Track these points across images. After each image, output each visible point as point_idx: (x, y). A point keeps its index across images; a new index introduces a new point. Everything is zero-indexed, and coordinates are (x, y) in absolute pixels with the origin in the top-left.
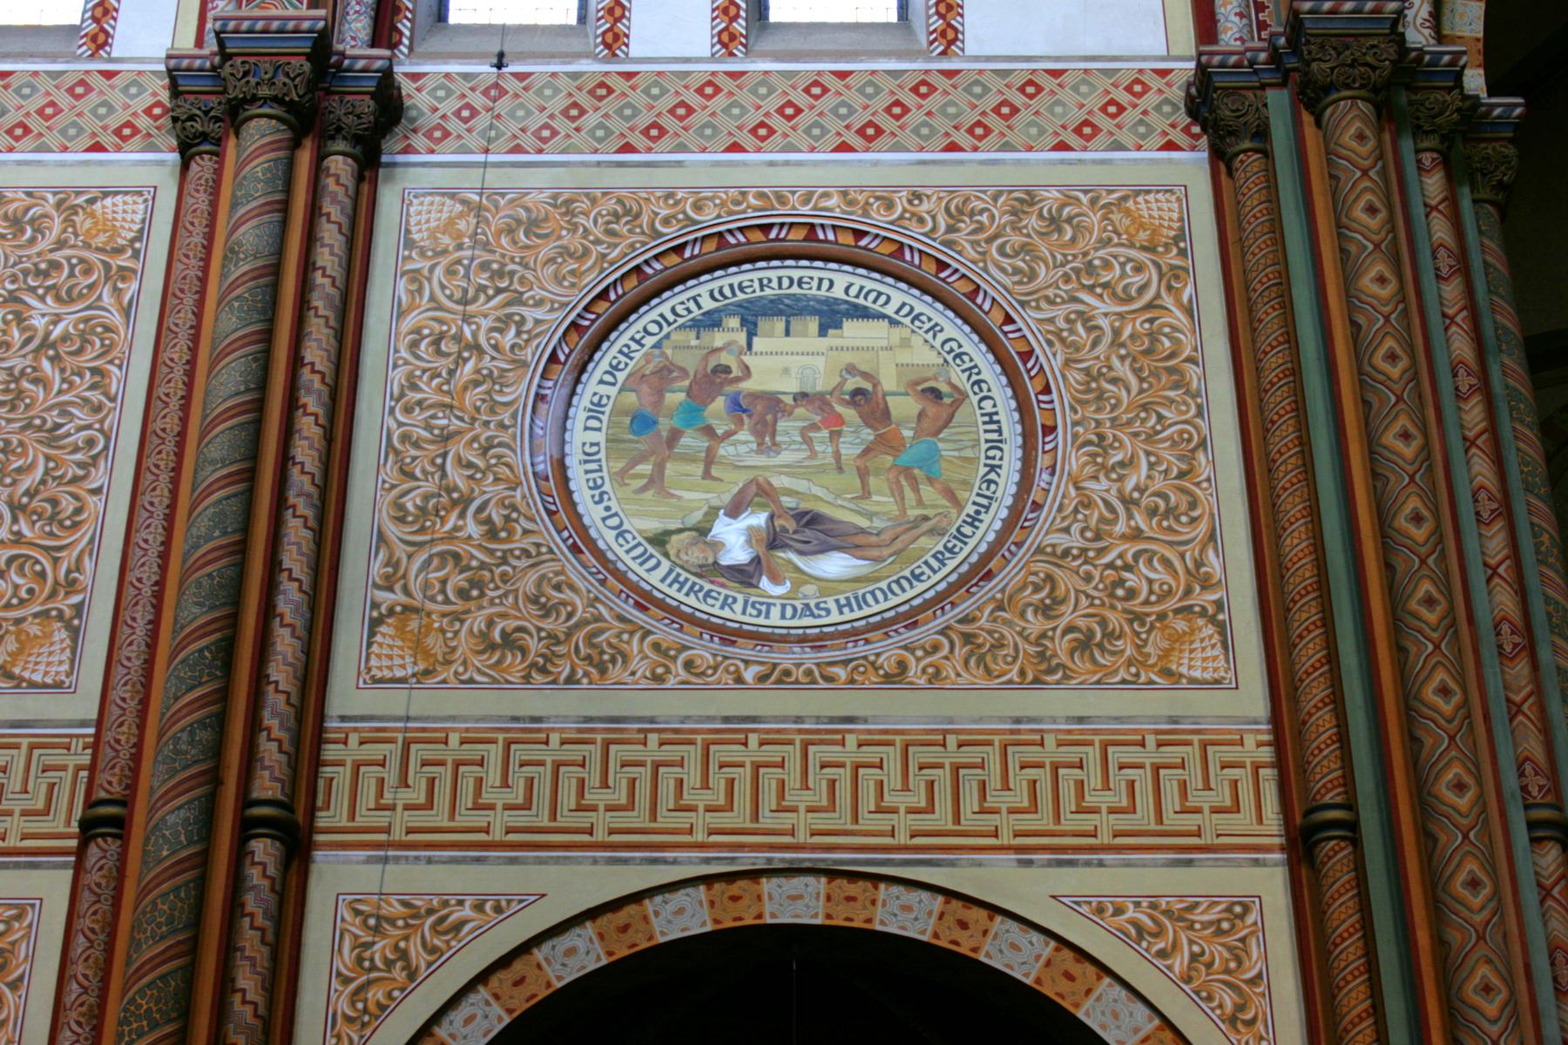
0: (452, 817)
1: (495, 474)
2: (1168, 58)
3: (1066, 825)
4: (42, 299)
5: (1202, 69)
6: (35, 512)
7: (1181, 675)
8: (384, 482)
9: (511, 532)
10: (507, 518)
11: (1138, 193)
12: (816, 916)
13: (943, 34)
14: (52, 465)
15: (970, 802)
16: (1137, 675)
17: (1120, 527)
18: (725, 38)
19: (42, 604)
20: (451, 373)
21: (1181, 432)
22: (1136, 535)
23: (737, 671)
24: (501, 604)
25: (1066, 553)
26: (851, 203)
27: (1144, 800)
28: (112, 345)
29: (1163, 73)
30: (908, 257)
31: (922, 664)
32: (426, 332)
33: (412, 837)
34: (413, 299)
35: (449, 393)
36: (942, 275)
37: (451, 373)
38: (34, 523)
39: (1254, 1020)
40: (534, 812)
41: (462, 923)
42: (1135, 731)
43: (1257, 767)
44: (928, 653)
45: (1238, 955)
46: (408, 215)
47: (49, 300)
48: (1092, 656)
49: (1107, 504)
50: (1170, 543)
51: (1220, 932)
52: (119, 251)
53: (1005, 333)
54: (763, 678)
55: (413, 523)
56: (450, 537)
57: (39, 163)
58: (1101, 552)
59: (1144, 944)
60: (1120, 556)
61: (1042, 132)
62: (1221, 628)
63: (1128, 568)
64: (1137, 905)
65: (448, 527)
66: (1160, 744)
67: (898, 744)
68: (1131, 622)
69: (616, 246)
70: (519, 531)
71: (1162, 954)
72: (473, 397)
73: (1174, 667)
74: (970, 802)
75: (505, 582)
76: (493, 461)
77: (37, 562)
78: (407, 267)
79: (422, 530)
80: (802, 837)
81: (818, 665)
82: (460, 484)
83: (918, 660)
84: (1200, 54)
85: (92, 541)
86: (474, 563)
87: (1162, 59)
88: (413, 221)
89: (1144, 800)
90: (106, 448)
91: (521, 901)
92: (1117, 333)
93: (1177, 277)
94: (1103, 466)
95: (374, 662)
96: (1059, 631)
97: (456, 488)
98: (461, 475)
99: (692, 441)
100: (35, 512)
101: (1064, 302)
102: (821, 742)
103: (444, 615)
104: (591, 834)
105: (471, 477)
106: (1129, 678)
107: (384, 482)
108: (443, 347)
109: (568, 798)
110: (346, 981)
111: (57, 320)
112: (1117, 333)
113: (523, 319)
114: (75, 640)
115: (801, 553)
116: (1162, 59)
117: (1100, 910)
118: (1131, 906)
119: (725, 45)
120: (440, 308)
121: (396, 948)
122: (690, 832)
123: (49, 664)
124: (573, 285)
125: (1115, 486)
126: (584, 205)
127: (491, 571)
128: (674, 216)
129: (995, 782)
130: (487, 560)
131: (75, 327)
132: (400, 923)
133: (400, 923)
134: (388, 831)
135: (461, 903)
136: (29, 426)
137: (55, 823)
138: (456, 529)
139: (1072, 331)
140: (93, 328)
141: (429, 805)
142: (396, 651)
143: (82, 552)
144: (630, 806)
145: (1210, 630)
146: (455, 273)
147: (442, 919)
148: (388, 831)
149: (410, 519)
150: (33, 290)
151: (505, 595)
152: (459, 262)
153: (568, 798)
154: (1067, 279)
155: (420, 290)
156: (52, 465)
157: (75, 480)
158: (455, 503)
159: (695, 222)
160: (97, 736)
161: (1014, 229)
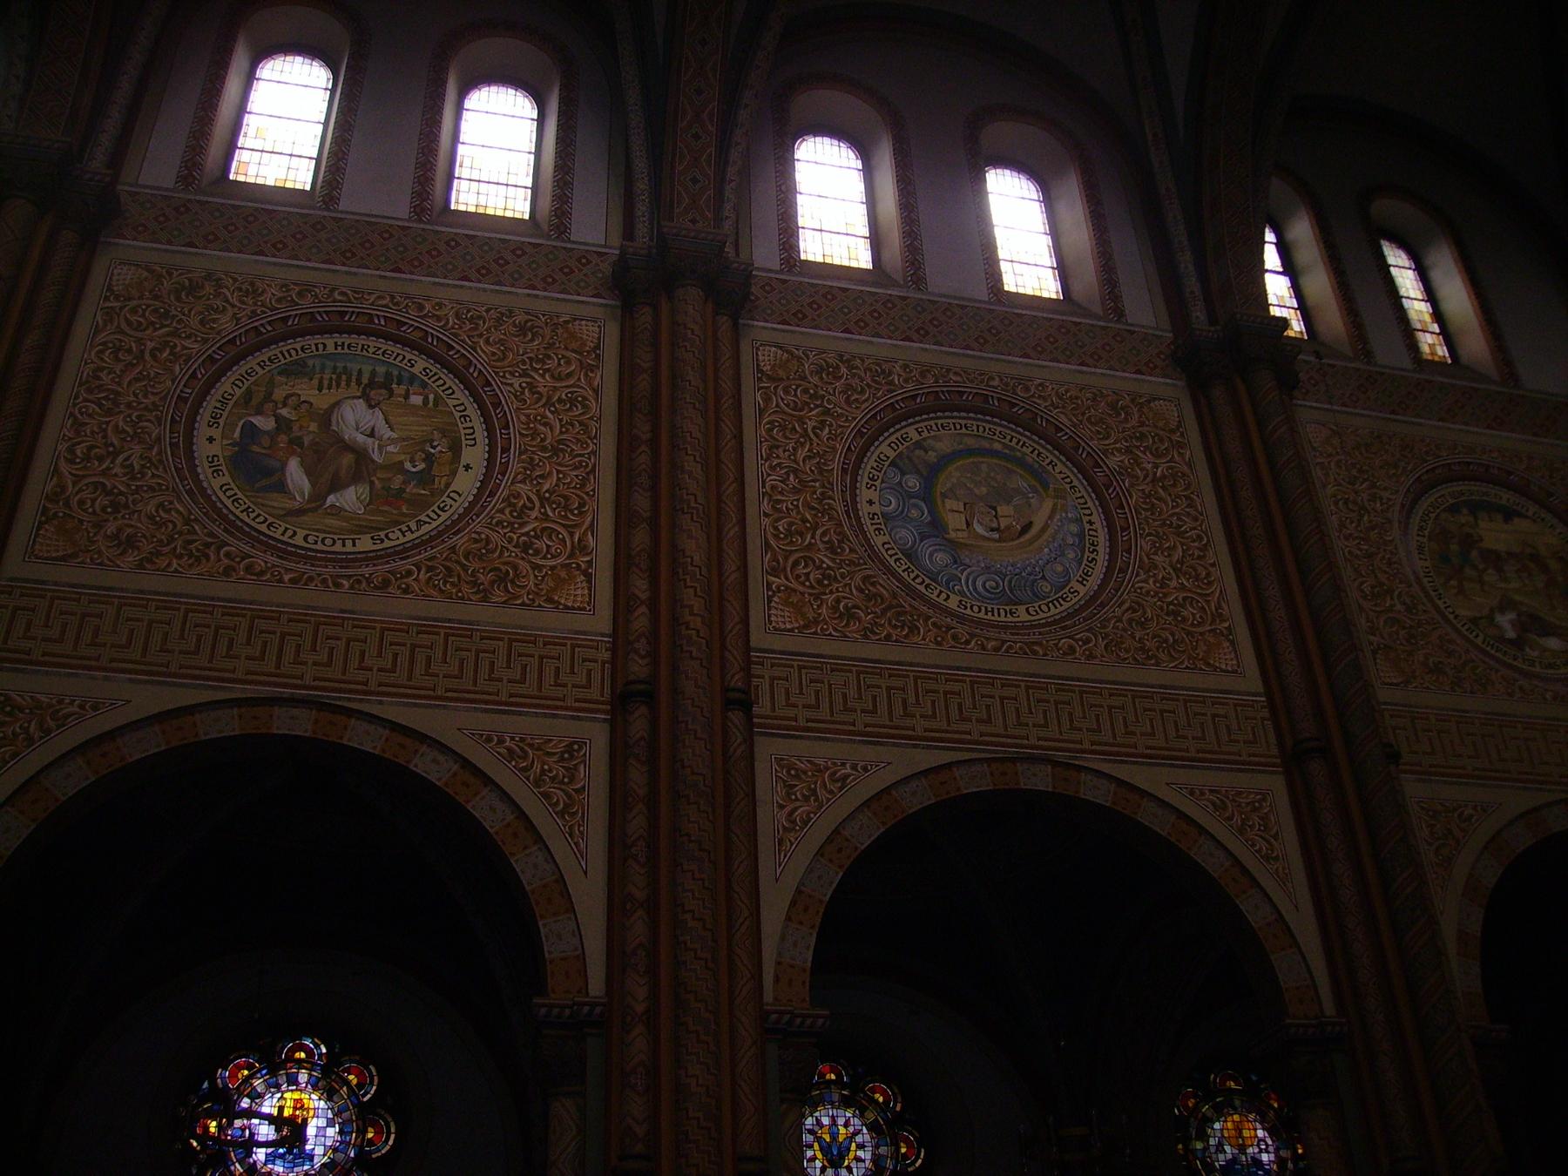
0: (210, 661)
1: (829, 514)
2: (605, 246)
3: (954, 727)
4: (543, 376)
5: (623, 255)
6: (554, 502)
7: (560, 604)
8: (64, 435)
9: (144, 475)
10: (143, 466)
11: (575, 320)
12: (306, 731)
13: (558, 227)
14: (561, 476)
15: (419, 668)
16: (533, 600)
17: (1174, 583)
18: (418, 210)
19: (1210, 625)
20: (1359, 521)
21: (580, 462)
22: (1183, 588)
23: (982, 644)
24: (129, 519)
25: (1148, 592)
26: (1007, 385)
27: (883, 707)
28: (1189, 484)
29: (600, 254)
30: (430, 340)
31: (398, 583)
32: (111, 345)
33: (316, 683)
34: (106, 325)
35: (1361, 531)
36: (451, 353)
37: (1359, 521)
38: (555, 509)
39: (575, 813)
40: (527, 685)
41: (847, 776)
42: (531, 635)
43: (604, 663)
44: (1085, 644)
45: (572, 774)
46: (112, 274)
47: (547, 376)
48: (506, 587)
49: (529, 499)
50: (564, 526)
51: (562, 759)
52: (1172, 431)
53: (485, 392)
54: (997, 649)
55: (79, 463)
56: (104, 473)
57: (462, 287)
58: (522, 525)
59: (513, 763)
60: (1176, 598)
61: (897, 329)
62: (588, 576)
63: (536, 537)
64: (512, 739)
65: (104, 466)
66: (545, 644)
67: (182, 610)
68: (533, 569)
69: (244, 309)
70: (150, 474)
71: (524, 769)
72: (1373, 535)
73: (556, 598)
74: (419, 668)
75: (844, 578)
76: (139, 431)
77: (560, 533)
78: (106, 305)
79: (85, 468)
80: (308, 681)
81: (331, 576)
82: (116, 442)
83: (1080, 647)
84: (622, 246)
85: (1221, 591)
86: (825, 565)
87: (601, 246)
88: (115, 278)
89: (883, 707)
90: (1208, 541)
91: (473, 734)
92: (549, 398)
93: (592, 371)
94: (530, 476)
95: (37, 547)
96: (488, 569)
97: (112, 445)
98: (810, 514)
99: (1468, 572)
100: (554, 502)
101: (520, 376)
102: (584, 646)
103: (810, 594)
104: (167, 667)
105: (816, 515)
106: (528, 602)
107: (64, 435)
108: (120, 355)
109: (549, 678)
110: (781, 807)
111: (1156, 466)
112: (549, 398)
113: (176, 345)
114: (589, 582)
115: (1538, 635)
116: (601, 246)
117: (489, 740)
118: (508, 739)
119: (417, 214)
120: (1340, 485)
121: (810, 789)
122: (98, 659)
123: (575, 596)
124: (857, 408)
125: (1167, 560)
126: (858, 362)
127: (126, 497)
128: (284, 297)
129: (912, 699)
130: (831, 564)
131: (566, 395)
132: (810, 773)
133: (810, 773)
134: (301, 678)
135: (843, 764)
136: (1164, 524)
137: (594, 693)
138: (108, 469)
139: (523, 393)
140: (576, 398)
141: (196, 652)
142: (787, 614)
143: (586, 530)
144: (329, 663)
145: (1226, 644)
146: (137, 312)
147: (835, 773)
148: (301, 678)
149: (78, 460)
150: (1138, 447)
151: (845, 585)
152: (139, 306)
153: (549, 678)
154: (524, 363)
155: (111, 321)
156: (104, 426)
157: (1199, 557)
158: (109, 453)
159: (298, 304)
160: (614, 643)
161: (496, 329)
